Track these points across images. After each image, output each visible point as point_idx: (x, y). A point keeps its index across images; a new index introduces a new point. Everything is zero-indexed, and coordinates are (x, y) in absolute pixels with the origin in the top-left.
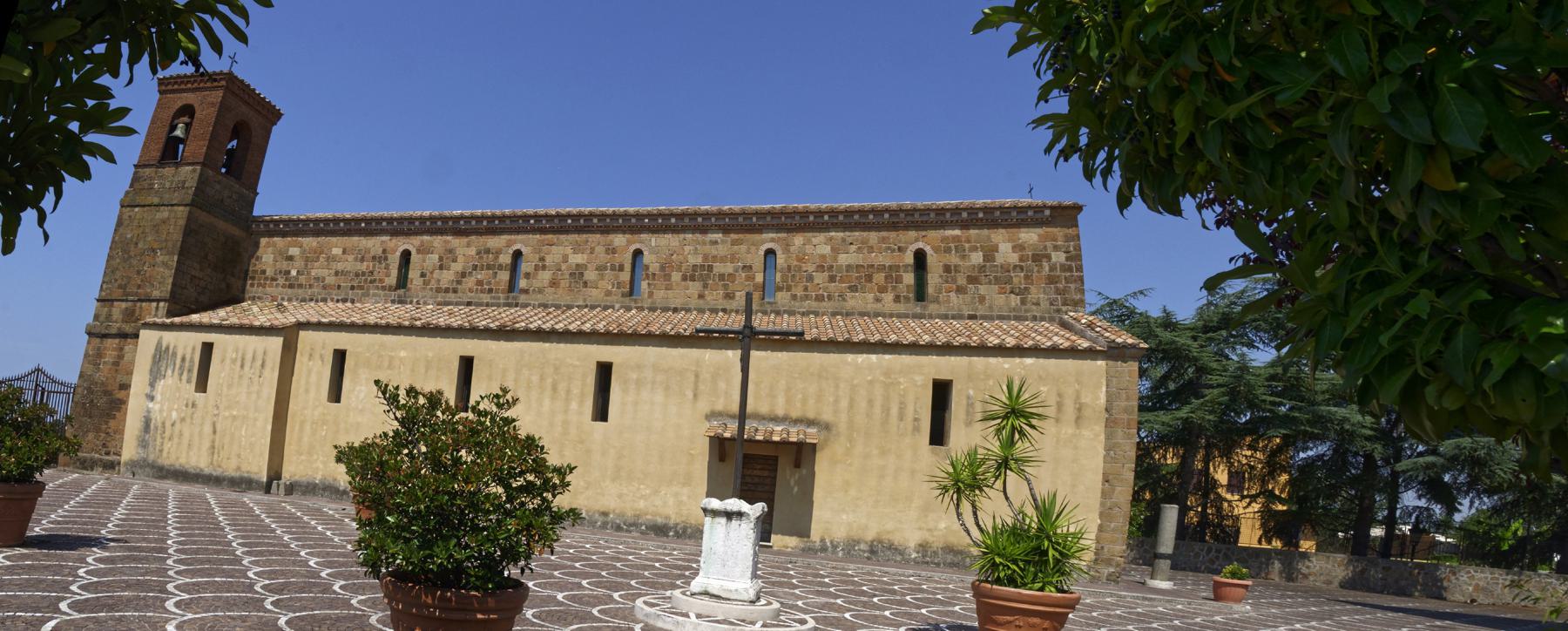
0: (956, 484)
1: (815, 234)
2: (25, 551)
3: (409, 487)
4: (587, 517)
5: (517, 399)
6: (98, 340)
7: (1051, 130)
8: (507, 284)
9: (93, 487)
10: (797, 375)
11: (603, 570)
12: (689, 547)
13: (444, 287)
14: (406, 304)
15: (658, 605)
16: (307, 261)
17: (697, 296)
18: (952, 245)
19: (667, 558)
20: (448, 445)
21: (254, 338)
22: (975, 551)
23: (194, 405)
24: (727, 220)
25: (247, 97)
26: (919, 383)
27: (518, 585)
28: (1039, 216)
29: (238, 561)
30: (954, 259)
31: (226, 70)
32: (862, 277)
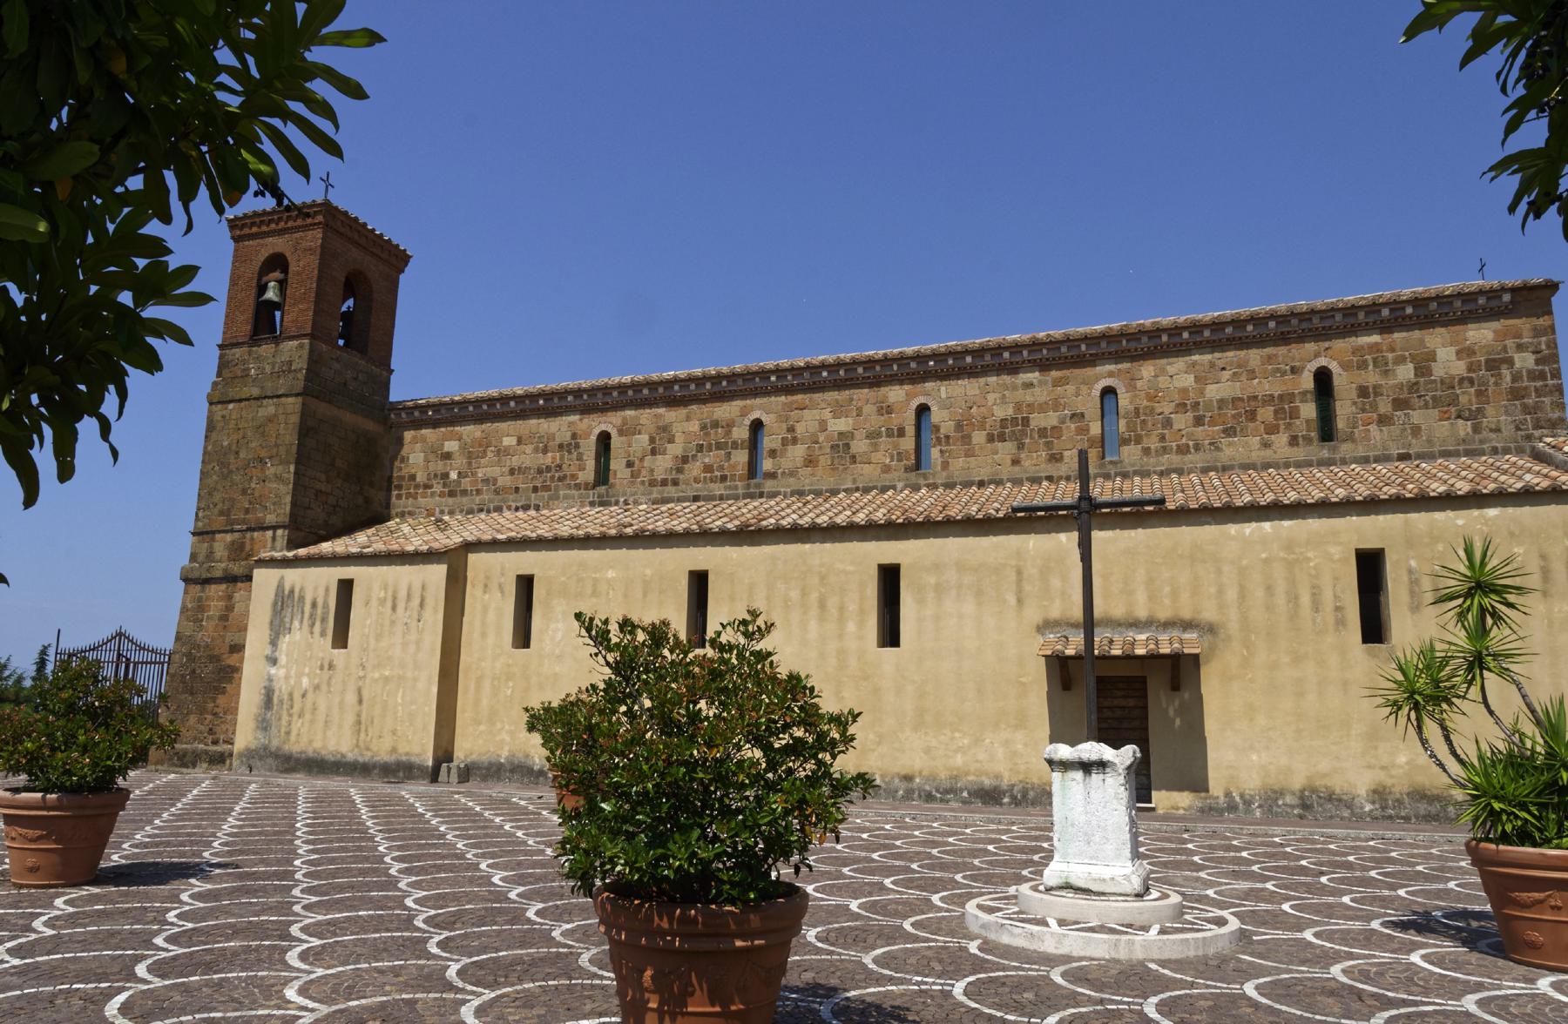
0: (1411, 697)
1: (1171, 360)
2: (95, 890)
3: (629, 759)
4: (883, 785)
5: (772, 624)
6: (198, 587)
7: (1518, 176)
8: (746, 468)
11: (913, 862)
12: (1036, 819)
15: (999, 909)
16: (469, 458)
17: (1009, 462)
20: (681, 696)
22: (1459, 794)
23: (331, 667)
24: (1045, 352)
25: (356, 237)
26: (1337, 557)
27: (791, 891)
28: (1494, 303)
29: (392, 883)
30: (1371, 377)
31: (319, 200)
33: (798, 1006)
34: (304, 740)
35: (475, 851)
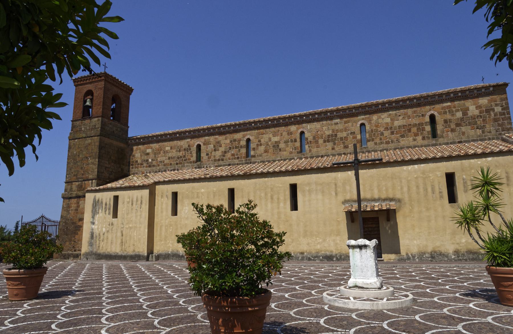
0: (466, 220)
2: (38, 301)
5: (256, 205)
6: (68, 200)
7: (493, 48)
9: (69, 267)
10: (381, 179)
11: (305, 280)
12: (344, 264)
13: (217, 159)
14: (202, 168)
15: (334, 295)
16: (155, 154)
17: (331, 149)
18: (447, 110)
19: (334, 271)
21: (136, 191)
23: (112, 224)
24: (341, 112)
26: (439, 176)
27: (266, 291)
29: (135, 294)
30: (448, 116)
31: (103, 72)
32: (406, 130)
33: (270, 329)
34: (104, 249)
35: (161, 283)
